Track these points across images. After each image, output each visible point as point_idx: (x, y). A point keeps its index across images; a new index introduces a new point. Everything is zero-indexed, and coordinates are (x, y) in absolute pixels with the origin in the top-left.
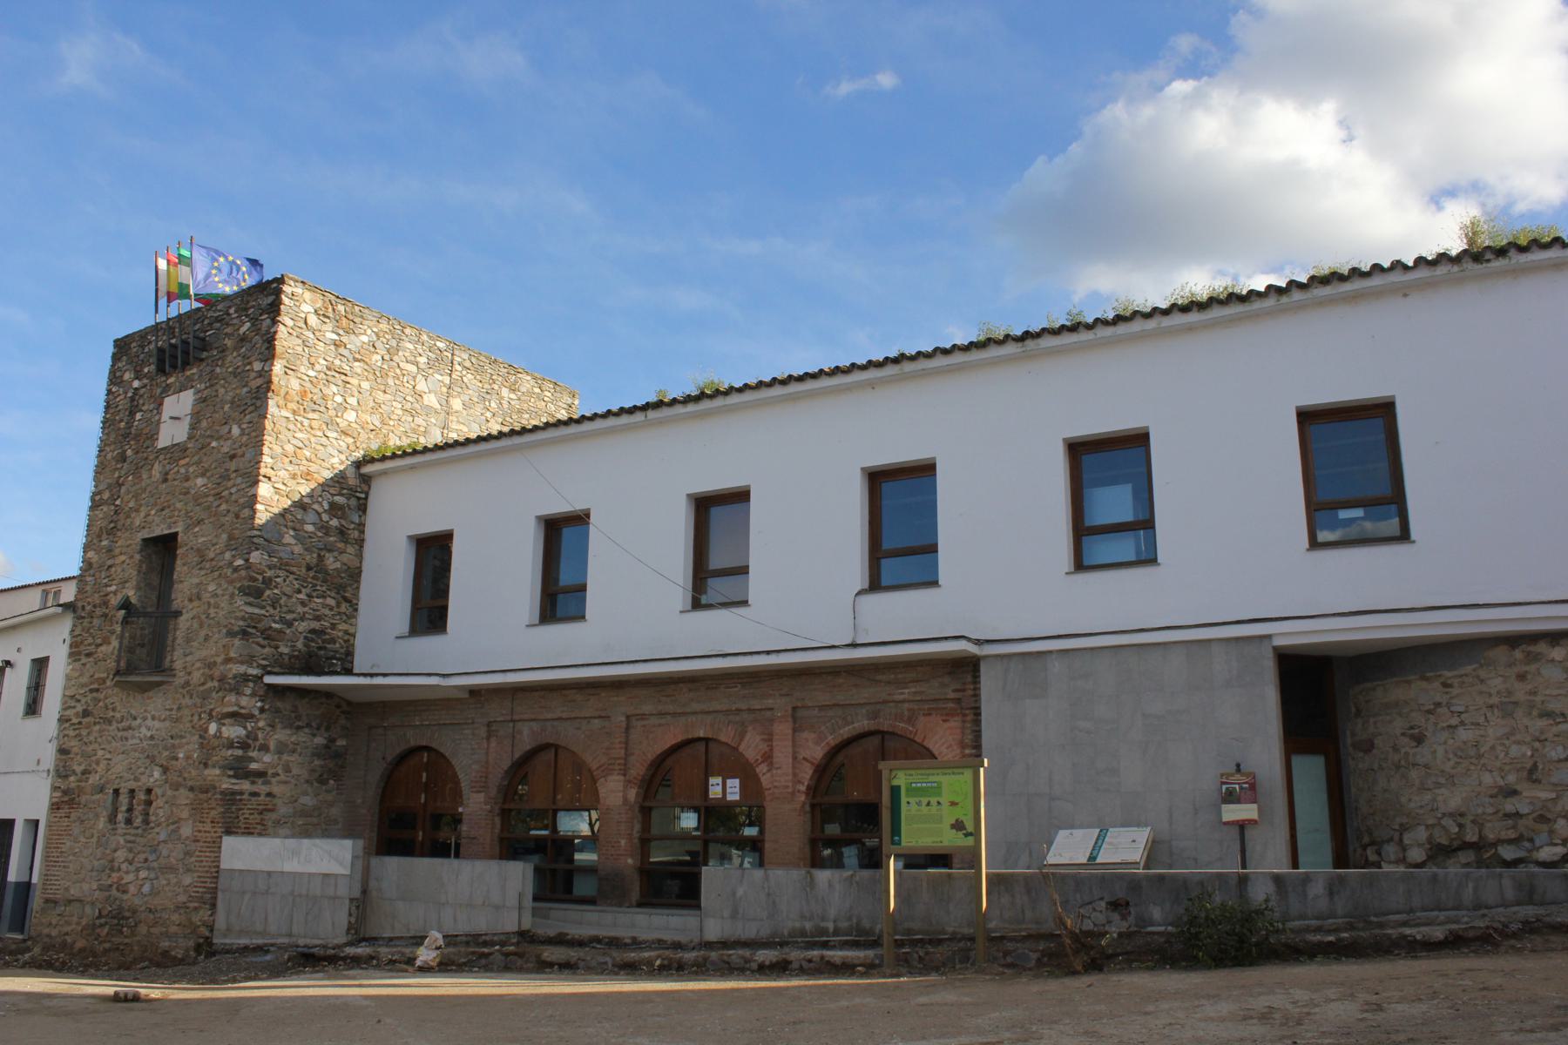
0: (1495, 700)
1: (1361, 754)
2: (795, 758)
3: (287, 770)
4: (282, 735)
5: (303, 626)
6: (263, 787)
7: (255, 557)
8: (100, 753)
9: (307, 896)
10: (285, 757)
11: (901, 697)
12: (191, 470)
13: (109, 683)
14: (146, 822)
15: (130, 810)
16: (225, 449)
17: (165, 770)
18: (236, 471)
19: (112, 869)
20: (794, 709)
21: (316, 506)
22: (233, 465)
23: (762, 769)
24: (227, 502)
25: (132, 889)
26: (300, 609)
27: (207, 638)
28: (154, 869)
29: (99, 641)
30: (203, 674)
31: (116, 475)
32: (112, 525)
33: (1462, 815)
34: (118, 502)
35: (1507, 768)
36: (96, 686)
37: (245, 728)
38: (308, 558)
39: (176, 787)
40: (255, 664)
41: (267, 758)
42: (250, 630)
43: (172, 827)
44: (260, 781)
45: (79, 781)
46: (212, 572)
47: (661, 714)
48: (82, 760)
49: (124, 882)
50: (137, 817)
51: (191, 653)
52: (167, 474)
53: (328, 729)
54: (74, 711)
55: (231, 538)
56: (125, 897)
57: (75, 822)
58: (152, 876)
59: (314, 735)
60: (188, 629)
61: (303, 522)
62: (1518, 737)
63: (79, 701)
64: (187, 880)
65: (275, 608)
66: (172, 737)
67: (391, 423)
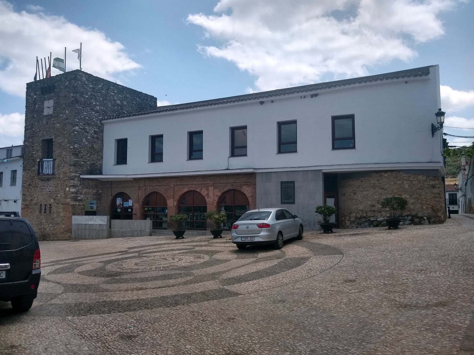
0: (372, 185)
1: (343, 196)
2: (214, 195)
3: (87, 199)
4: (85, 190)
5: (89, 163)
6: (81, 203)
7: (76, 146)
8: (35, 195)
9: (96, 229)
10: (86, 196)
11: (238, 181)
12: (55, 122)
13: (36, 177)
14: (50, 212)
15: (45, 209)
16: (65, 117)
17: (55, 199)
18: (68, 123)
19: (41, 224)
20: (214, 184)
21: (90, 132)
22: (67, 121)
23: (206, 197)
24: (66, 131)
25: (48, 229)
26: (88, 158)
27: (64, 166)
28: (53, 224)
29: (32, 166)
30: (63, 175)
31: (32, 122)
32: (32, 135)
33: (363, 211)
34: (33, 129)
35: (373, 200)
36: (32, 178)
37: (76, 189)
38: (89, 145)
39: (58, 204)
40: (78, 173)
41: (82, 196)
42: (76, 164)
43: (58, 214)
44: (81, 202)
45: (30, 202)
46: (64, 149)
47: (182, 185)
48: (30, 197)
49: (45, 227)
50: (47, 211)
51: (60, 170)
52: (48, 122)
53: (97, 188)
54: (26, 184)
55: (68, 140)
56: (46, 231)
57: (29, 213)
58: (53, 226)
59: (93, 190)
60: (58, 164)
61: (87, 136)
62: (376, 194)
63: (27, 182)
64: (63, 226)
65: (82, 159)
66: (56, 191)
67: (108, 109)
